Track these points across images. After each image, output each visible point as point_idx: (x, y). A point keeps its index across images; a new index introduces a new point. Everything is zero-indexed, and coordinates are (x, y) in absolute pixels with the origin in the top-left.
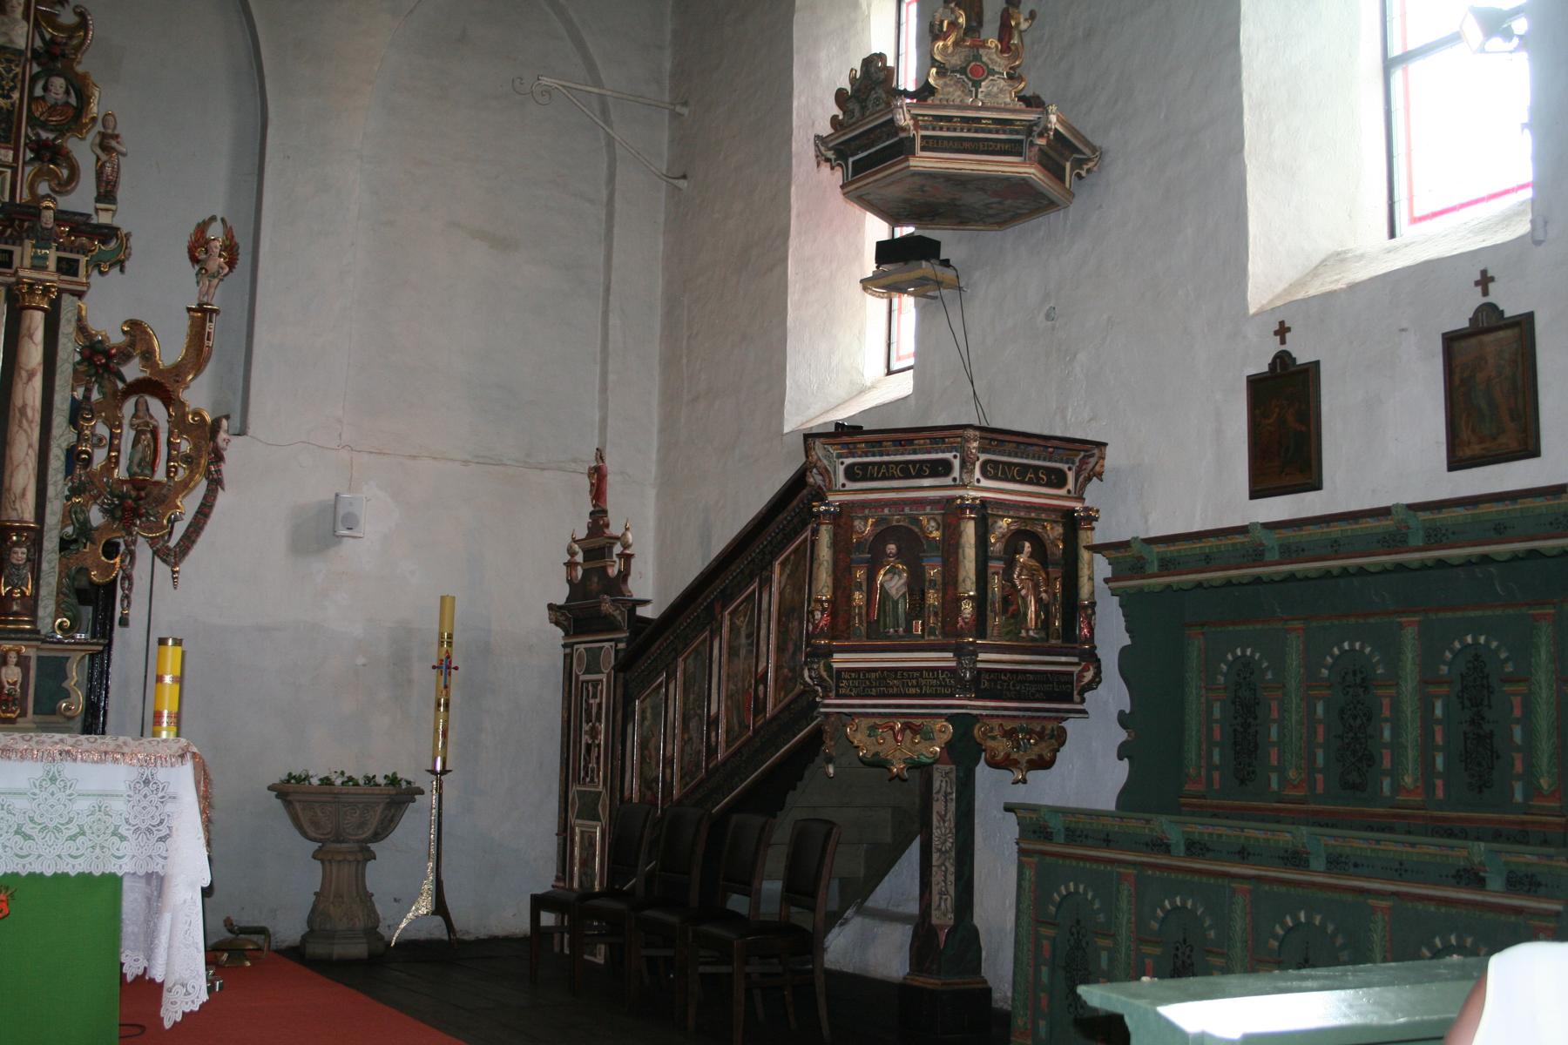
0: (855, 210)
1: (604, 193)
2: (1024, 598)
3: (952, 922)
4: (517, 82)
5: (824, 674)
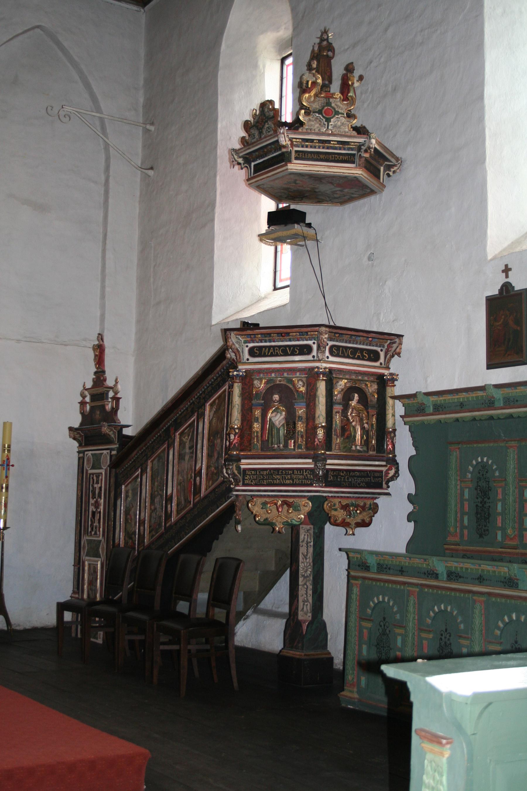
0: (254, 194)
1: (103, 178)
2: (354, 427)
3: (310, 618)
4: (49, 108)
5: (236, 472)
